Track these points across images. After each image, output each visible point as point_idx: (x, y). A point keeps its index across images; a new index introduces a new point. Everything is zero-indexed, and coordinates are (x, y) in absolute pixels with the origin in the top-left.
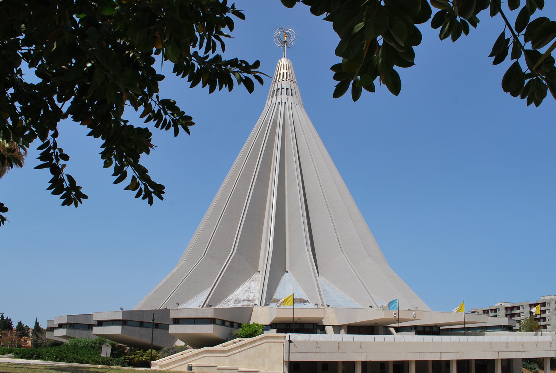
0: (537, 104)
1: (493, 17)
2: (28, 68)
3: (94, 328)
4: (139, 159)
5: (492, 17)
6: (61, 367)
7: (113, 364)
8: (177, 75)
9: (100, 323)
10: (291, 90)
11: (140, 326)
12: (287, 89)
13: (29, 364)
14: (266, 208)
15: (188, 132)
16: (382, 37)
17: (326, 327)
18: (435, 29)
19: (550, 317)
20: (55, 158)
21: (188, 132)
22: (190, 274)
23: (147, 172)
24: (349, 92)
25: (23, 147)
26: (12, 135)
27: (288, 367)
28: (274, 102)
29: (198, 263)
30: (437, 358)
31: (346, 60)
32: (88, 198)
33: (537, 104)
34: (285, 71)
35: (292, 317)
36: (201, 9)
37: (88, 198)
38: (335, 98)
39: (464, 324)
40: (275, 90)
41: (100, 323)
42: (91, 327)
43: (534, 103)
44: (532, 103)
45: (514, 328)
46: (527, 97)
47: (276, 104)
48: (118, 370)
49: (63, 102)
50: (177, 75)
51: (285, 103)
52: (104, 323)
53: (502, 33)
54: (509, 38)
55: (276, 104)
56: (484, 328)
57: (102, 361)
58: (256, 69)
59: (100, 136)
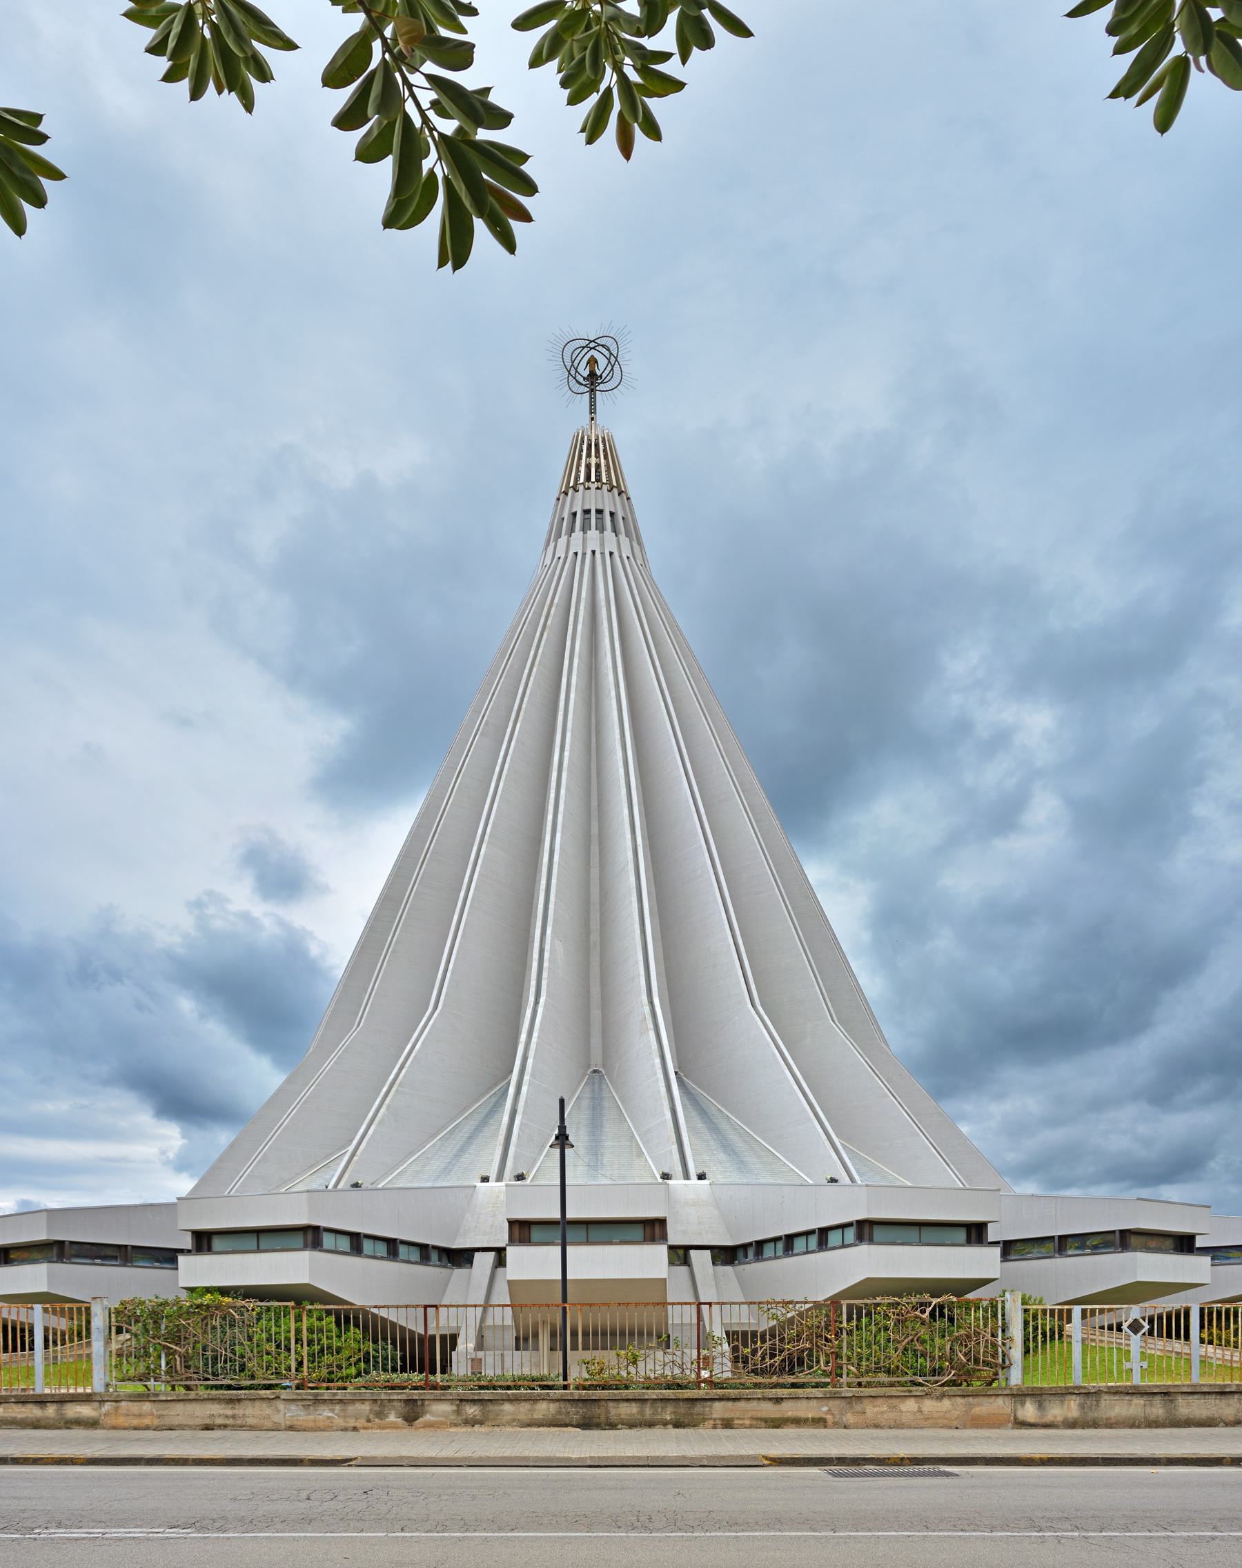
0: (38, 118)
1: (325, 88)
2: (341, 11)
3: (181, 1259)
4: (423, 161)
5: (323, 86)
6: (445, 152)
7: (294, 1540)
8: (454, 270)
9: (203, 1241)
10: (612, 514)
11: (318, 1245)
12: (599, 512)
13: (458, 1118)
14: (575, 660)
15: (510, 245)
16: (450, 1325)
17: (477, 1255)
18: (713, 46)
19: (562, 1102)
20: (156, 4)
21: (510, 245)
22: (403, 905)
23: (344, 11)
24: (256, 84)
25: (31, 1338)
26: (1178, 37)
27: (388, 215)
28: (561, 553)
29: (680, 660)
30: (43, 1330)
31: (177, 1254)
32: (477, 14)
33: (38, 118)
34: (593, 460)
35: (551, 1282)
36: (1227, 10)
37: (477, 14)
38: (1129, 97)
39: (665, 1304)
40: (563, 519)
41: (203, 1241)
42: (205, 1242)
43: (695, 48)
44: (522, 170)
45: (1199, 1243)
46: (23, 203)
47: (566, 558)
48: (387, 1384)
49: (437, 139)
50: (454, 270)
51: (594, 552)
52: (217, 1243)
53: (686, 61)
54: (608, 84)
55: (566, 558)
56: (186, 1251)
57: (1170, 1423)
58: (643, 131)
59: (390, 24)
